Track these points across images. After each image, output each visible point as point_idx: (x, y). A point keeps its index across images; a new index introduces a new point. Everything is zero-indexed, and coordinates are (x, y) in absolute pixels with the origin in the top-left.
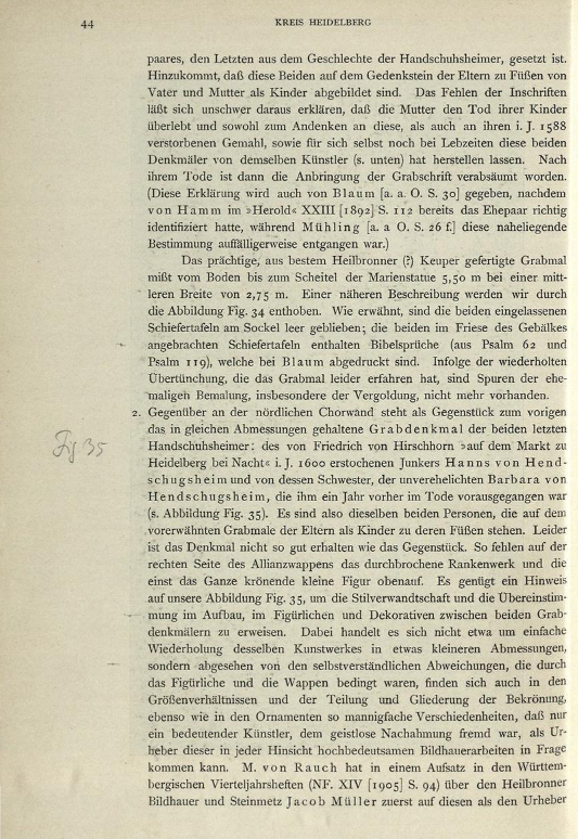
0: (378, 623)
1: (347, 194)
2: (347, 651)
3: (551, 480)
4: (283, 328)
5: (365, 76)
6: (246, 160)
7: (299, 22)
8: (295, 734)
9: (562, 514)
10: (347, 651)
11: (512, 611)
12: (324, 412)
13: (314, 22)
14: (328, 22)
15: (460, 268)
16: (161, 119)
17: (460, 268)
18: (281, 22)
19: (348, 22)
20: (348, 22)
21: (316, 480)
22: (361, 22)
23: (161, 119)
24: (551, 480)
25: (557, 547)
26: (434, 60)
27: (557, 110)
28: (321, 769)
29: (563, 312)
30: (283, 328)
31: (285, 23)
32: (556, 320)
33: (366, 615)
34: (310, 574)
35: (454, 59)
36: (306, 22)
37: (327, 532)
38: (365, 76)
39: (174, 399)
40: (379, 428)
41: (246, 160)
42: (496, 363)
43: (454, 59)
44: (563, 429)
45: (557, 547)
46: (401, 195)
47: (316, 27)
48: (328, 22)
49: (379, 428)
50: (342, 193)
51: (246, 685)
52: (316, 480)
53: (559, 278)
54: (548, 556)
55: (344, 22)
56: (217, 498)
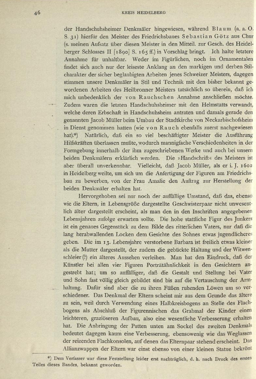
0: (111, 208)
1: (219, 29)
6: (114, 37)
8: (142, 319)
9: (249, 280)
12: (244, 36)
13: (138, 13)
14: (146, 13)
18: (124, 13)
19: (155, 13)
20: (155, 13)
21: (183, 74)
25: (248, 257)
26: (91, 30)
27: (249, 59)
28: (171, 128)
29: (249, 302)
31: (126, 13)
32: (246, 215)
35: (140, 29)
40: (219, 36)
41: (114, 37)
42: (143, 243)
43: (140, 29)
44: (250, 318)
45: (248, 257)
46: (244, 29)
47: (141, 15)
48: (146, 13)
50: (216, 28)
52: (183, 74)
53: (248, 143)
54: (243, 262)
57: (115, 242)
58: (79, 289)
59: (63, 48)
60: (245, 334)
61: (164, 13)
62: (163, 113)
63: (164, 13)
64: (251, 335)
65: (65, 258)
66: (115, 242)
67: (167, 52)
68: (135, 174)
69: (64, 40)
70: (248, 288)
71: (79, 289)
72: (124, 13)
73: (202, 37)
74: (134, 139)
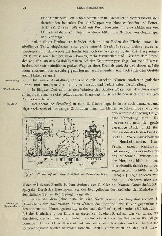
2: (118, 123)
3: (140, 61)
4: (58, 56)
5: (142, 151)
7: (84, 8)
10: (118, 123)
11: (149, 184)
14: (91, 8)
15: (131, 68)
16: (25, 216)
17: (131, 68)
18: (79, 8)
22: (101, 8)
23: (25, 216)
24: (140, 61)
30: (58, 56)
31: (80, 8)
33: (110, 223)
34: (126, 63)
36: (86, 8)
37: (142, 199)
38: (142, 151)
39: (147, 219)
40: (107, 46)
48: (91, 8)
49: (107, 46)
51: (133, 66)
55: (96, 7)
56: (145, 52)
57: (139, 156)
58: (136, 170)
59: (22, 216)
60: (154, 156)
61: (103, 8)
62: (134, 23)
63: (103, 8)
64: (158, 191)
65: (133, 47)
66: (139, 156)
67: (132, 18)
68: (136, 104)
69: (53, 125)
70: (156, 184)
71: (136, 170)
72: (79, 8)
73: (141, 52)
74: (135, 216)
